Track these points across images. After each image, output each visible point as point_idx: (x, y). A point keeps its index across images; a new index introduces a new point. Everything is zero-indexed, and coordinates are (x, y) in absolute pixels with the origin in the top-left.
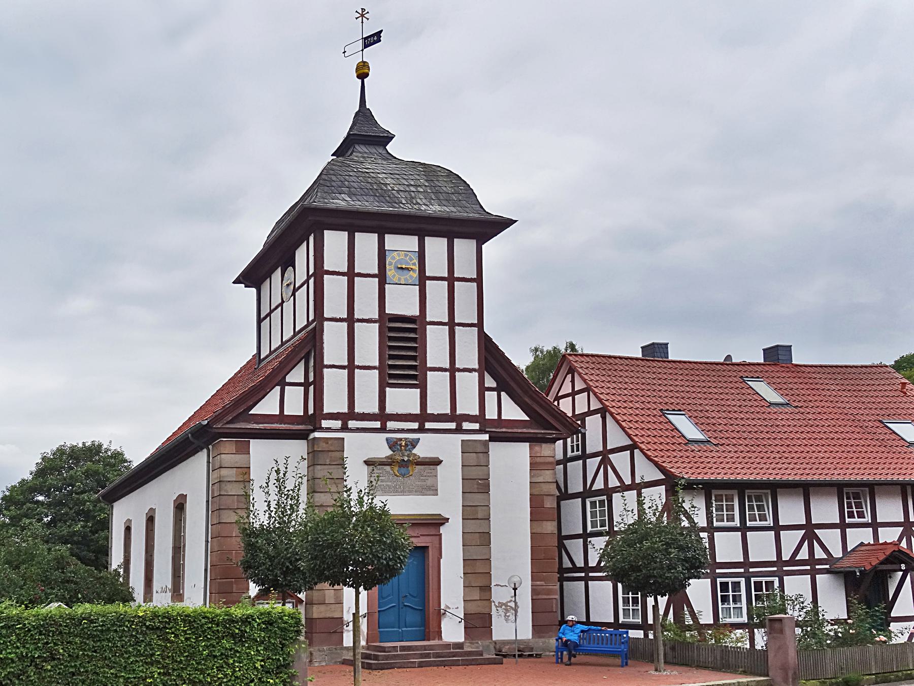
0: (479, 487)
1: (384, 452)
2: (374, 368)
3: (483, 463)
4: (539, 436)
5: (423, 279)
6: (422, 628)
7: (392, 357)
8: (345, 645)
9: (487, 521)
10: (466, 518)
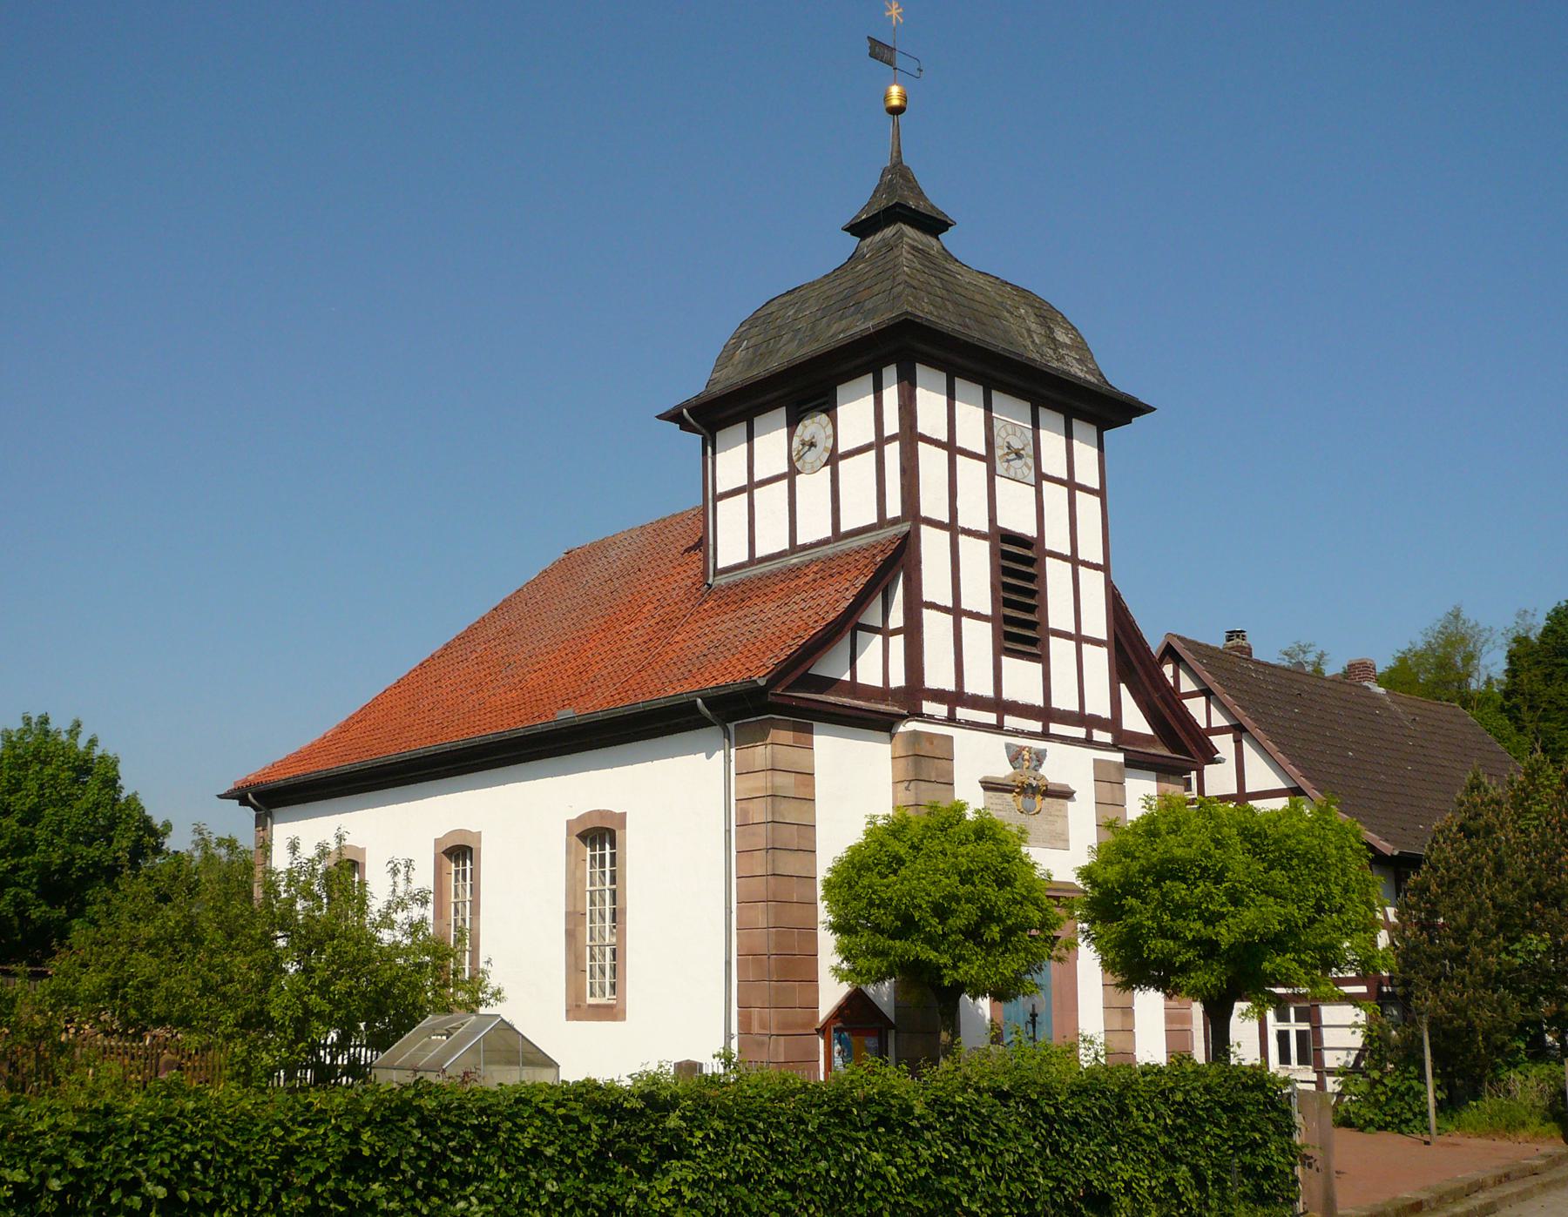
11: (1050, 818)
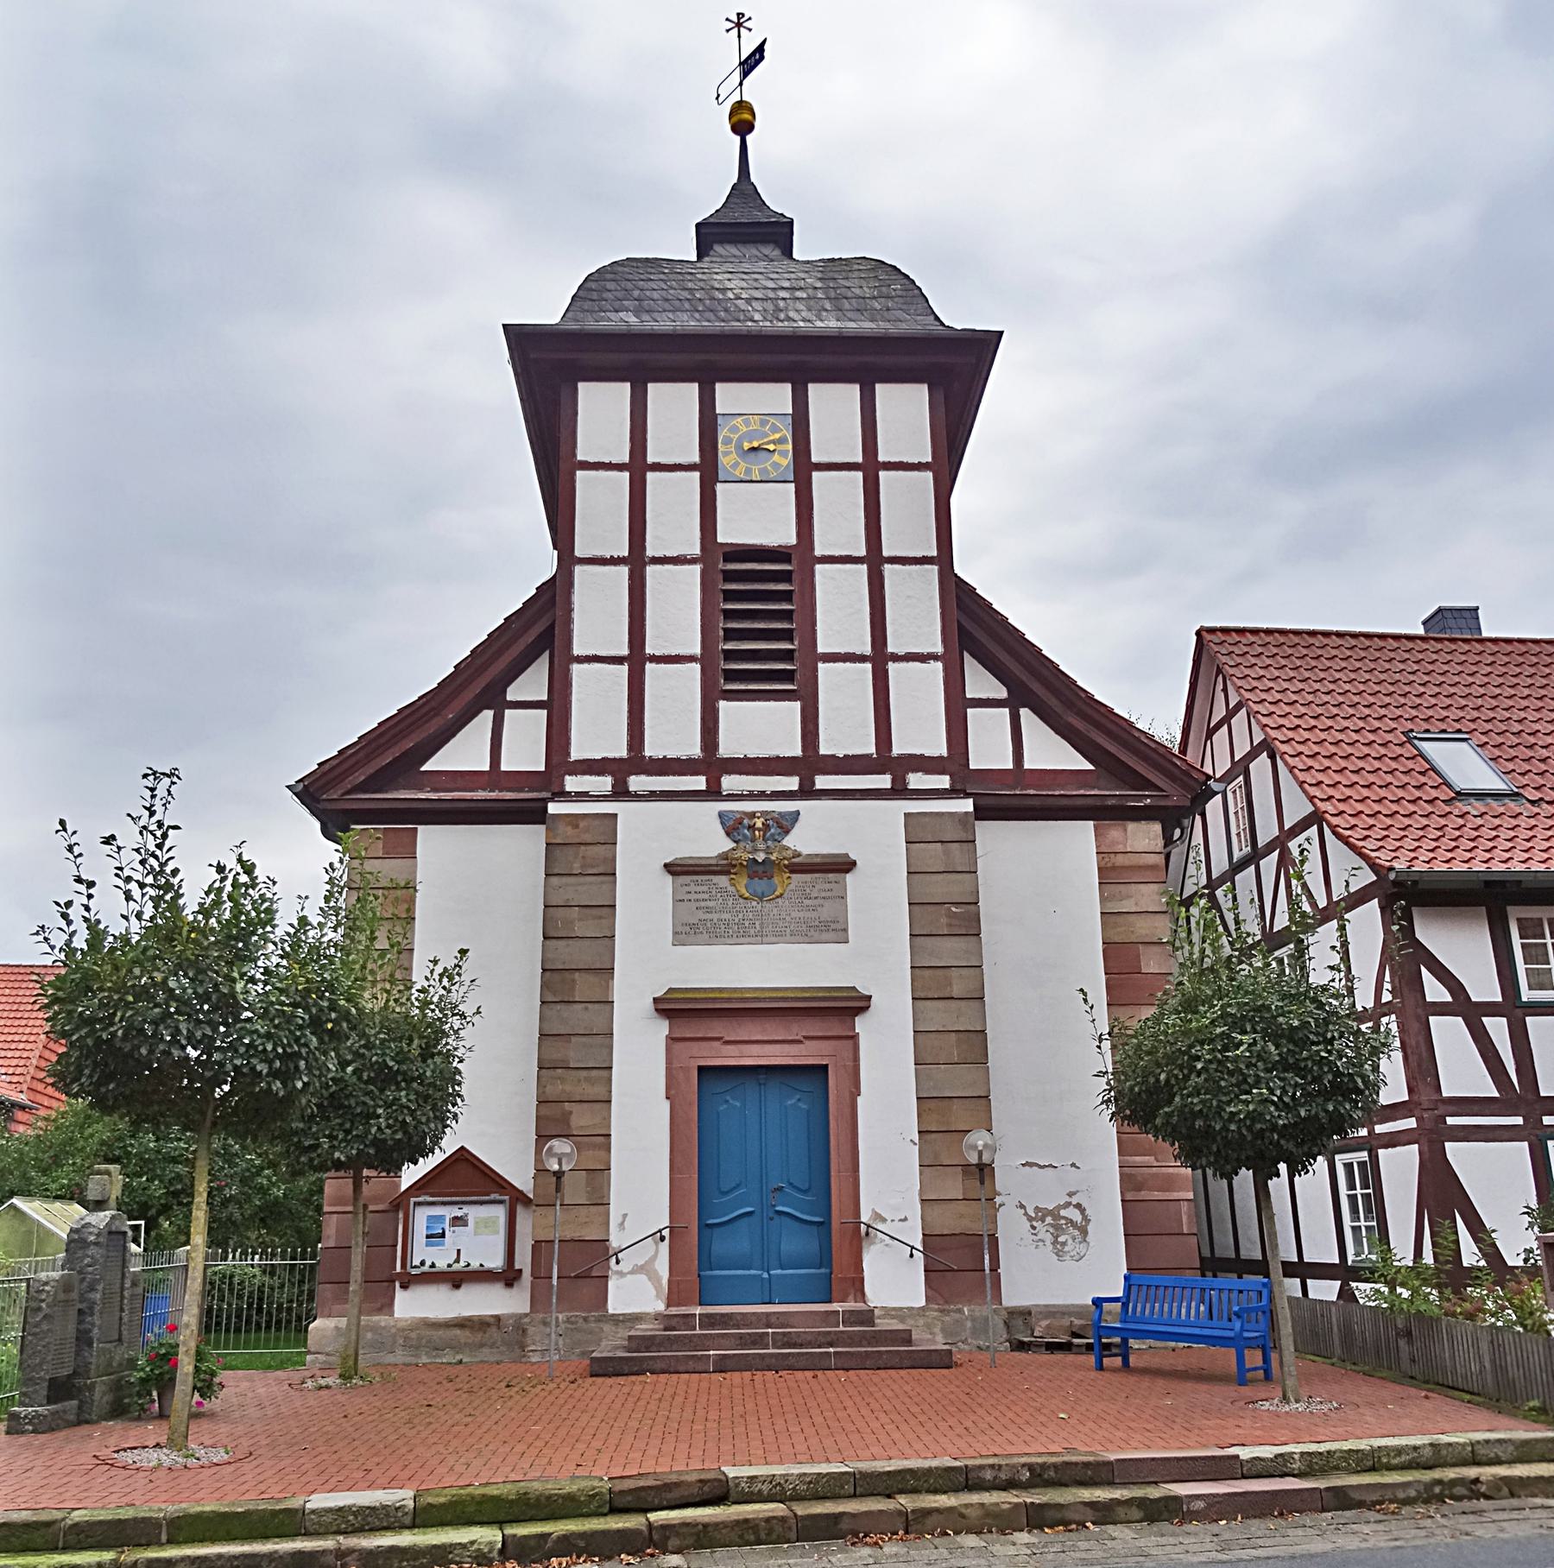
0: (954, 922)
1: (713, 843)
2: (691, 659)
3: (960, 863)
4: (1110, 802)
5: (803, 470)
6: (823, 1270)
7: (730, 635)
8: (611, 1311)
9: (976, 1004)
10: (923, 996)
11: (807, 902)
